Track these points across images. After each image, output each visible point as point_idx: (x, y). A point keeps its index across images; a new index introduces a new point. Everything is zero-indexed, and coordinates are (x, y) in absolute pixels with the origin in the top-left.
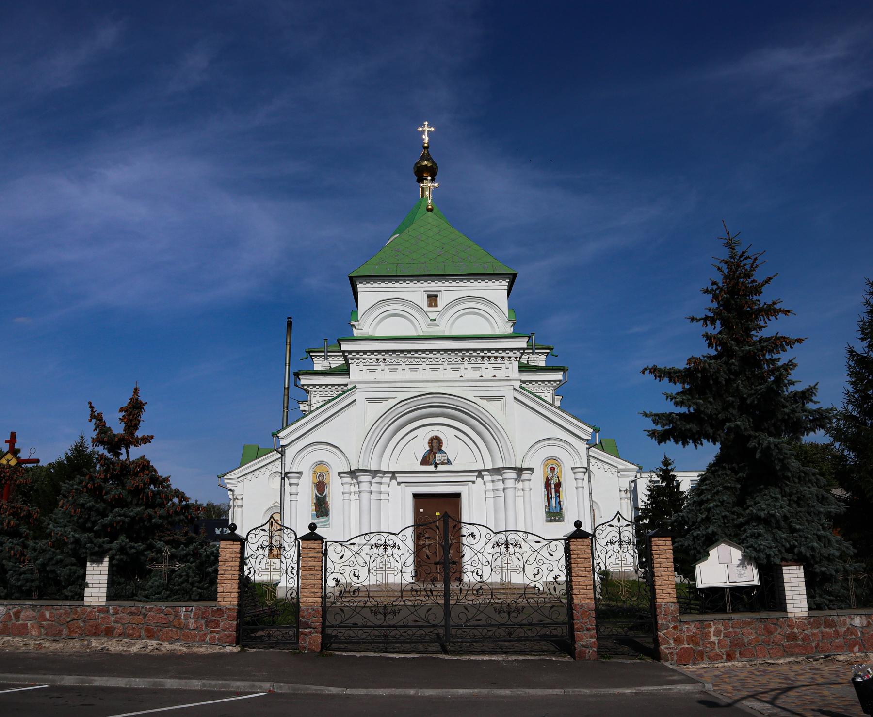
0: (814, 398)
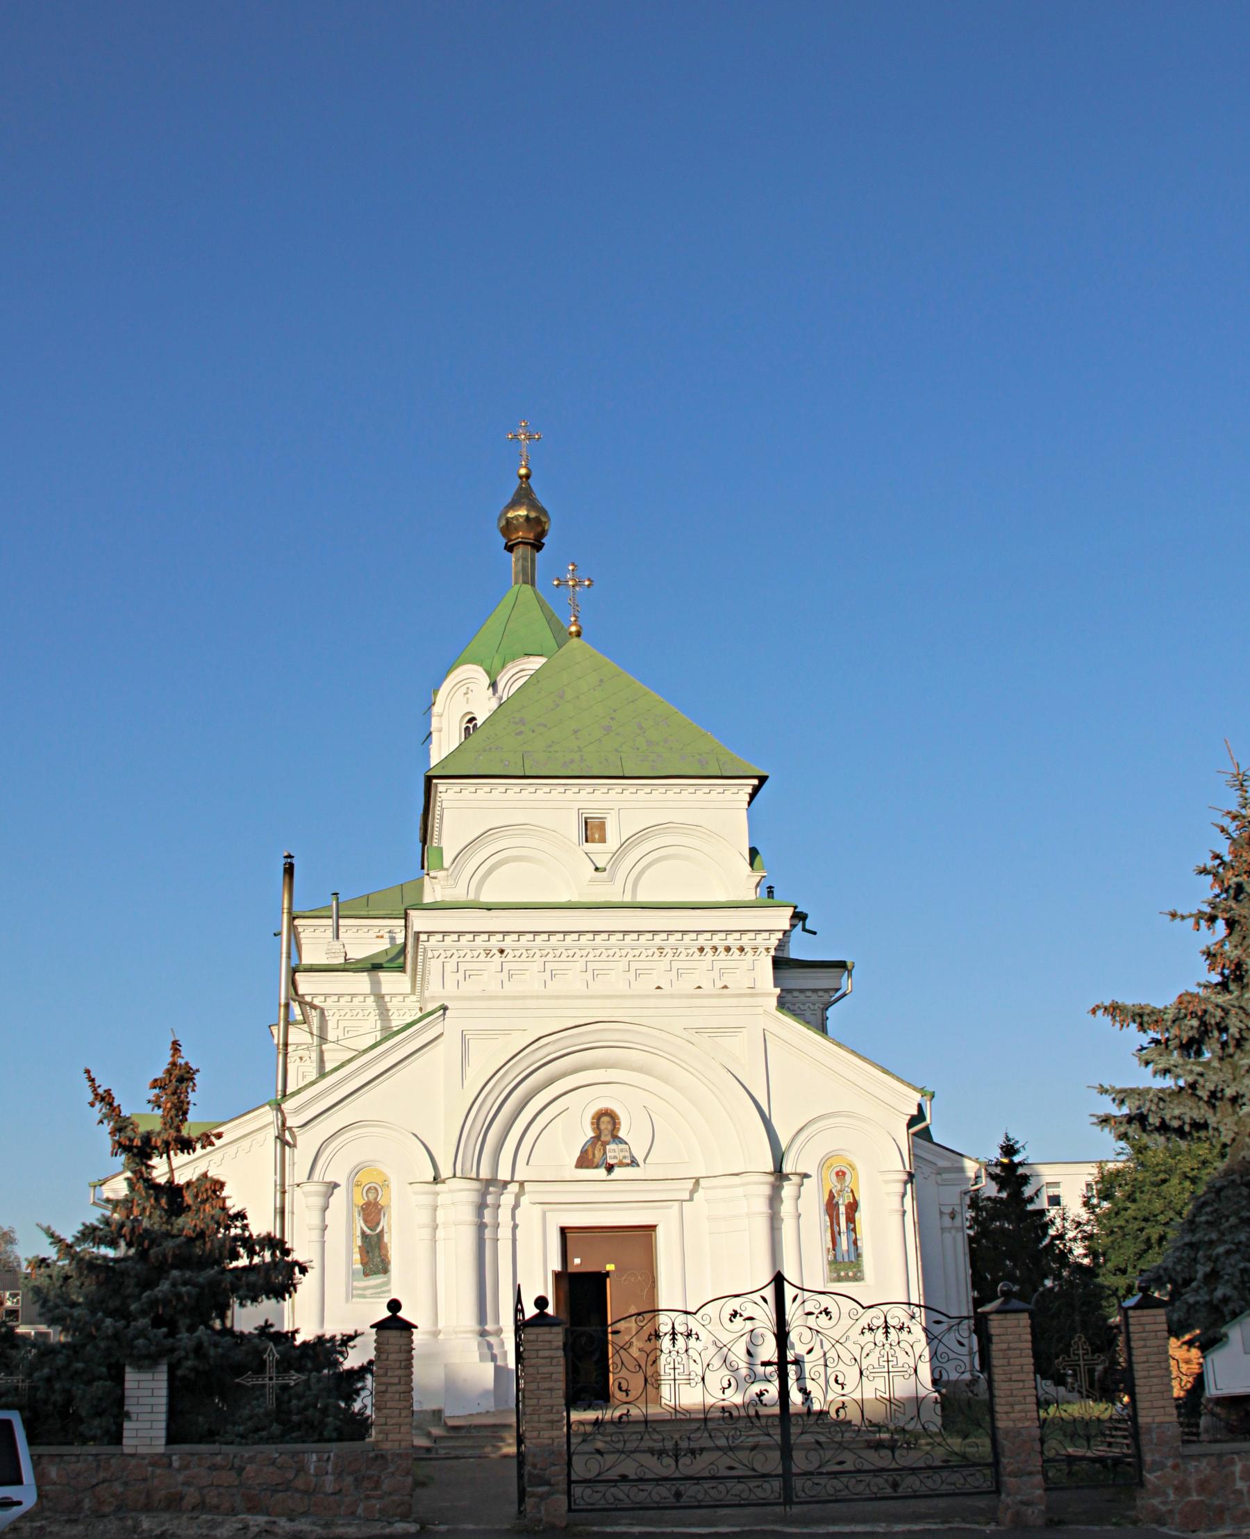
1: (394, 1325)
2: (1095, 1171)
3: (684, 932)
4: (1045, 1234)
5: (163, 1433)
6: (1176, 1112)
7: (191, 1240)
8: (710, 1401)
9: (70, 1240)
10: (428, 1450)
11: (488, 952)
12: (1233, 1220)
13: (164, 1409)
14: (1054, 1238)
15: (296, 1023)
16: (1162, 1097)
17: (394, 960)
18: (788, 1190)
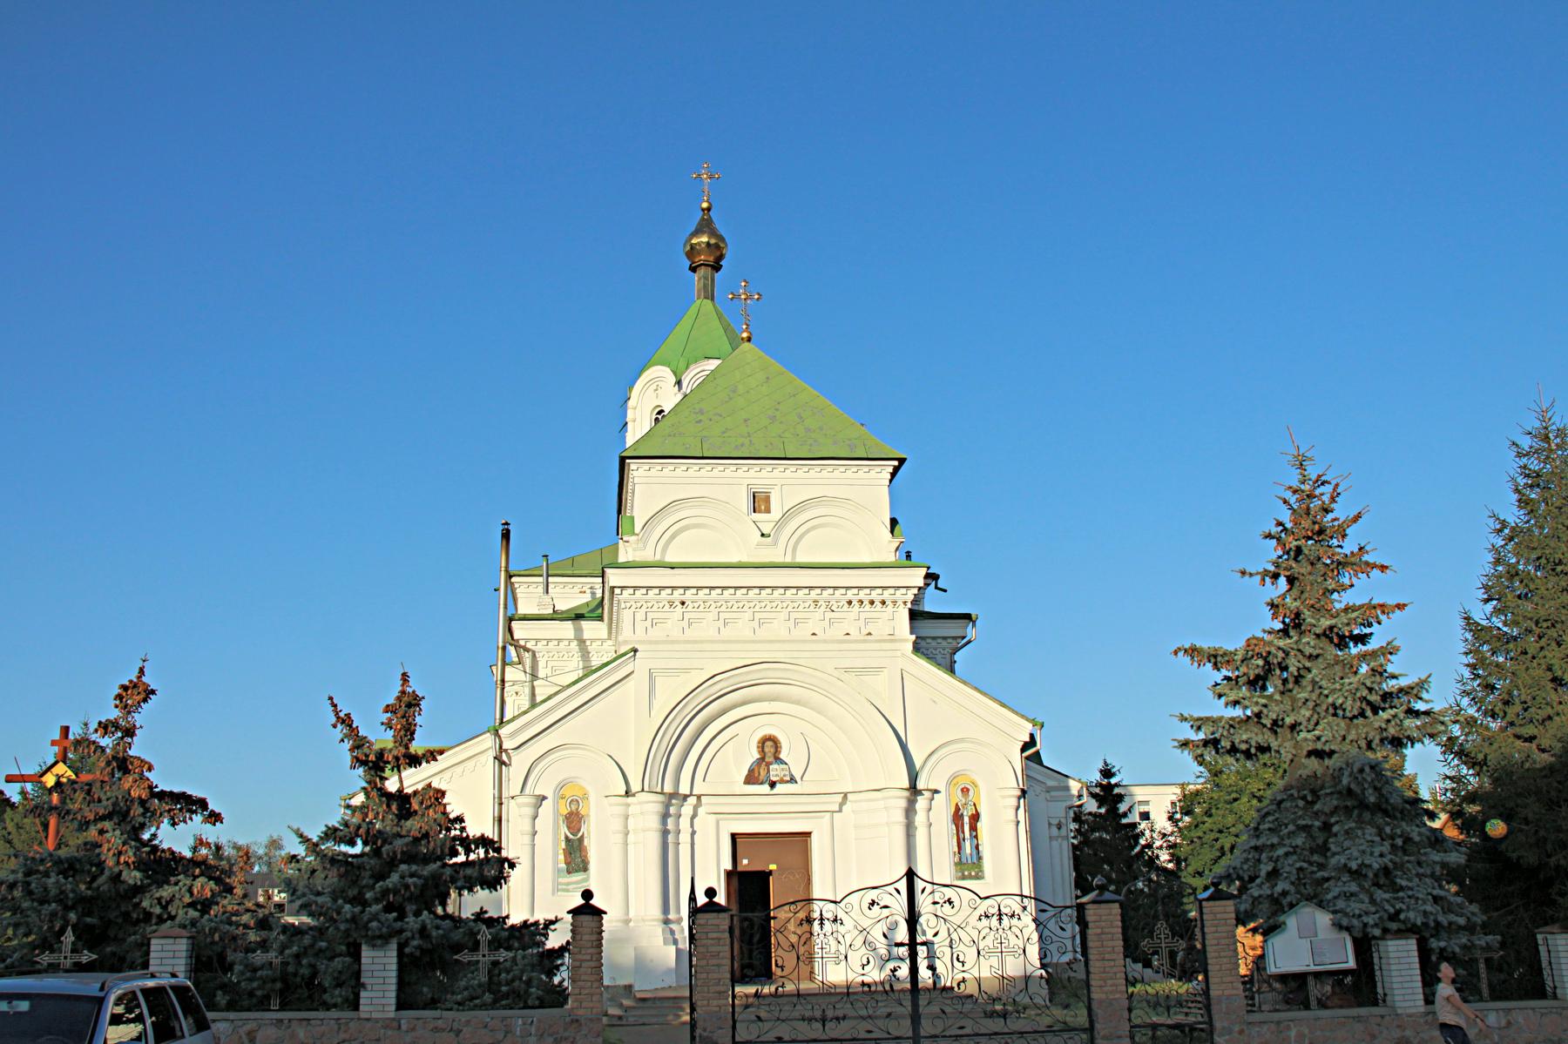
0: (1424, 695)
1: (587, 911)
2: (1178, 791)
3: (835, 588)
4: (1137, 843)
5: (393, 1001)
6: (1242, 736)
7: (416, 840)
8: (851, 976)
9: (315, 839)
10: (620, 1018)
11: (671, 603)
12: (1291, 827)
13: (394, 981)
14: (1144, 847)
15: (512, 664)
16: (1233, 724)
17: (594, 611)
18: (921, 803)
